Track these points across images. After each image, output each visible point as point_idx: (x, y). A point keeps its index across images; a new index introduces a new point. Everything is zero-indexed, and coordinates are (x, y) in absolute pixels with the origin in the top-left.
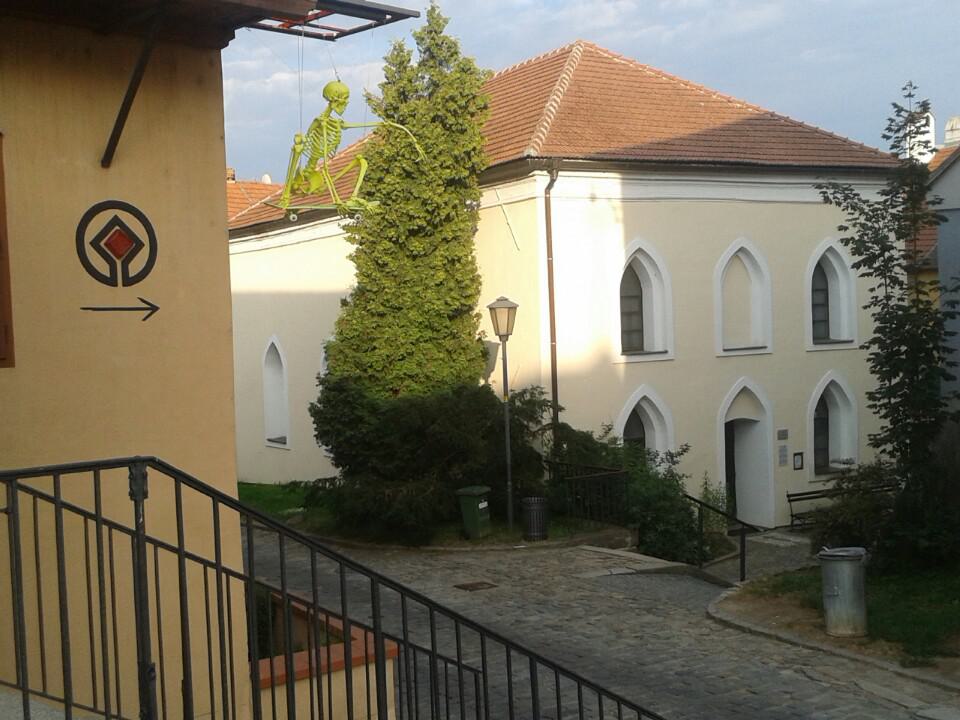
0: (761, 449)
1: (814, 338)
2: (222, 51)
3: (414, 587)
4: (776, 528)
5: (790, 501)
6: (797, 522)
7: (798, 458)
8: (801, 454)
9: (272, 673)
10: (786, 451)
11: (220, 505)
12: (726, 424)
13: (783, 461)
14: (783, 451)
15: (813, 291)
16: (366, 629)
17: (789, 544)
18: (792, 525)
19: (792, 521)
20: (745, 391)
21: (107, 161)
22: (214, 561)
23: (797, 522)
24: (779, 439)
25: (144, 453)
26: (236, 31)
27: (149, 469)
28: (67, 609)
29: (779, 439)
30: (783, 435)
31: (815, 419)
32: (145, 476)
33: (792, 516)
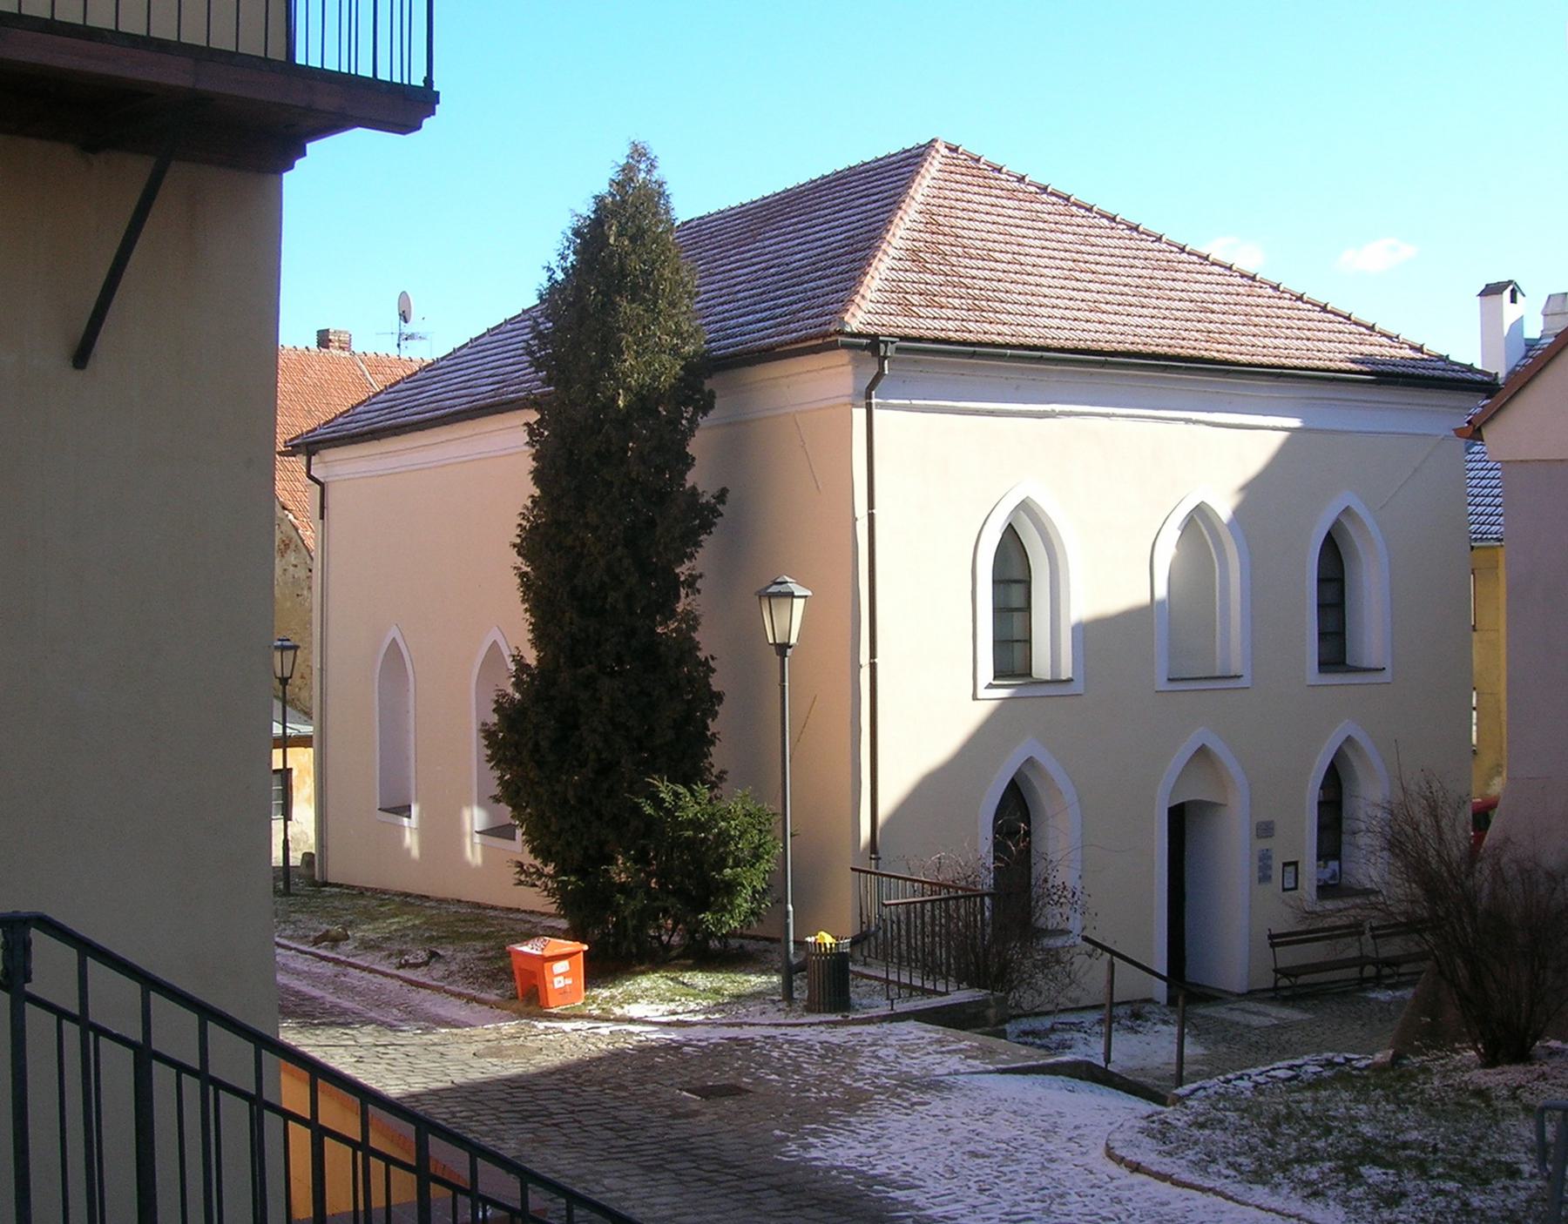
0: (1232, 850)
1: (1320, 664)
2: (286, 176)
3: (487, 1142)
4: (1250, 992)
5: (1273, 945)
6: (1284, 982)
7: (1291, 869)
8: (1295, 864)
9: (1111, 982)
10: (1270, 857)
11: (153, 995)
12: (1171, 810)
13: (1265, 878)
14: (1265, 859)
15: (1319, 580)
16: (456, 1189)
17: (1266, 1021)
18: (1276, 988)
19: (1276, 981)
20: (1202, 753)
21: (81, 356)
22: (197, 1067)
23: (1284, 982)
24: (1259, 837)
25: (26, 907)
26: (309, 146)
27: (35, 934)
28: (15, 1135)
29: (1259, 837)
30: (1265, 830)
31: (1320, 803)
32: (27, 945)
33: (1276, 971)
